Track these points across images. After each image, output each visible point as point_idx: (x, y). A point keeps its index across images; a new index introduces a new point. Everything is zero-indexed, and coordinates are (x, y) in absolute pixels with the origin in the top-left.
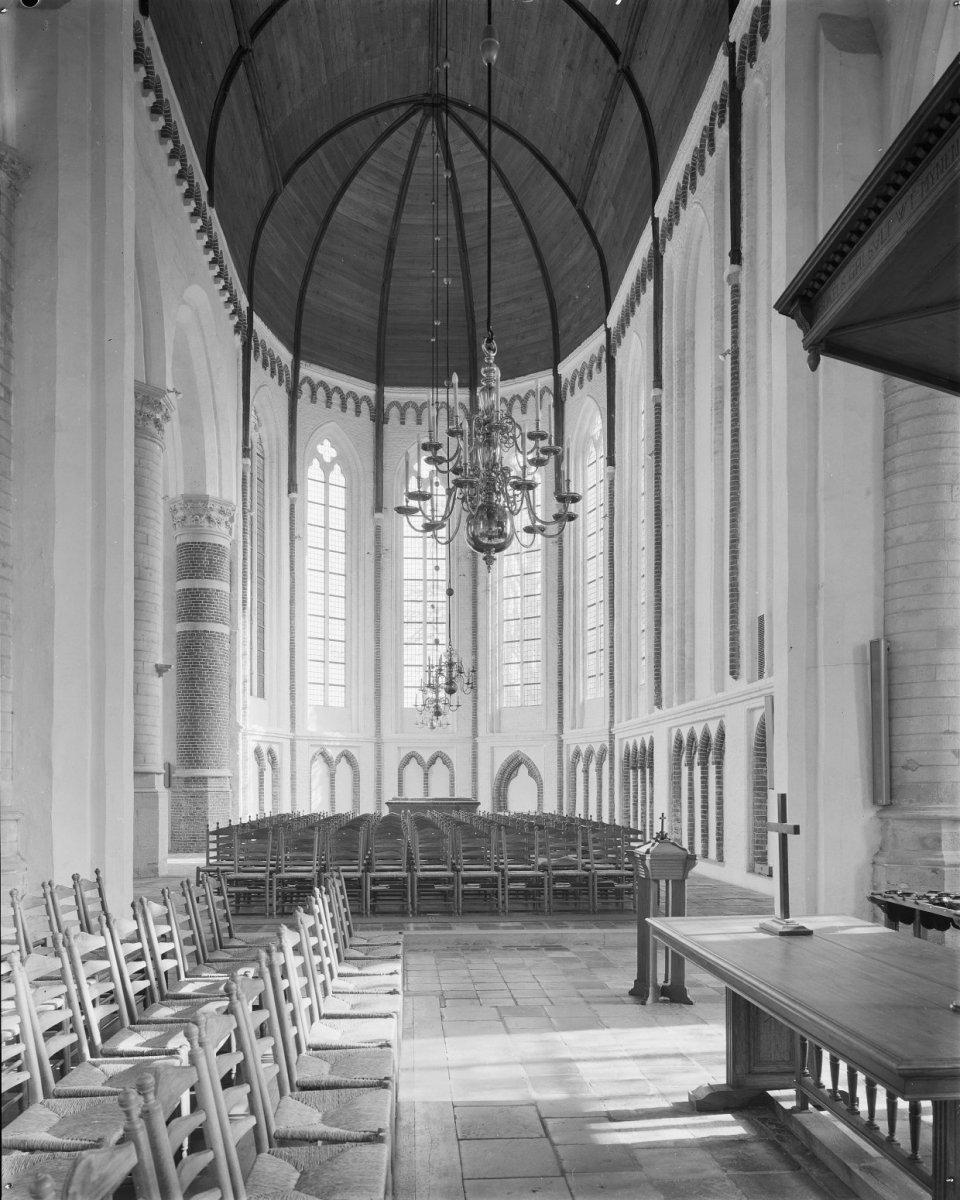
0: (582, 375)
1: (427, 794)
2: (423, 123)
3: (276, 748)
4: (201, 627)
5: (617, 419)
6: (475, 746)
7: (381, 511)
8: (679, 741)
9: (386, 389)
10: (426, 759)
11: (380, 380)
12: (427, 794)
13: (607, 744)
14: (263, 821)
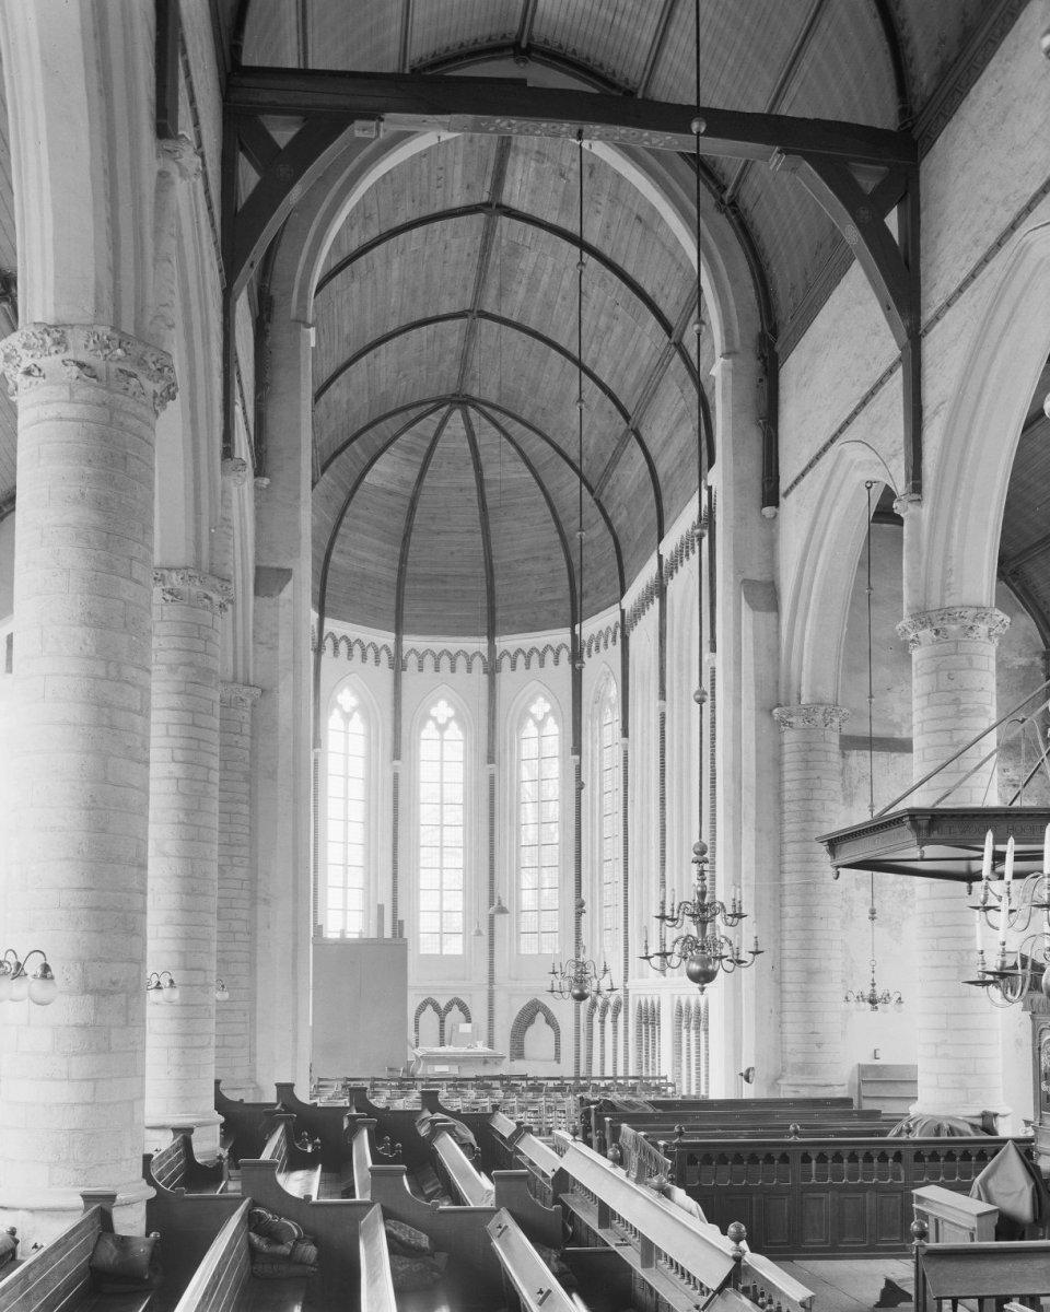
0: (599, 641)
2: (449, 413)
9: (405, 637)
10: (443, 1005)
13: (622, 998)
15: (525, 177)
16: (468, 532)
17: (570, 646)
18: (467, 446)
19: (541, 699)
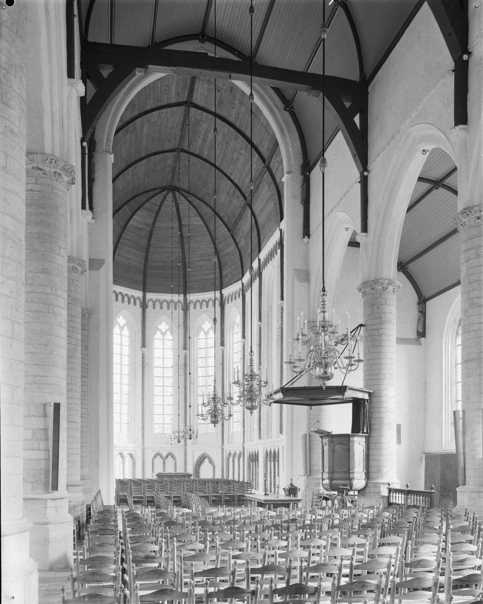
0: (232, 297)
1: (176, 471)
2: (167, 194)
5: (246, 320)
6: (186, 450)
7: (145, 347)
8: (267, 452)
10: (164, 455)
11: (145, 291)
13: (242, 451)
19: (207, 322)
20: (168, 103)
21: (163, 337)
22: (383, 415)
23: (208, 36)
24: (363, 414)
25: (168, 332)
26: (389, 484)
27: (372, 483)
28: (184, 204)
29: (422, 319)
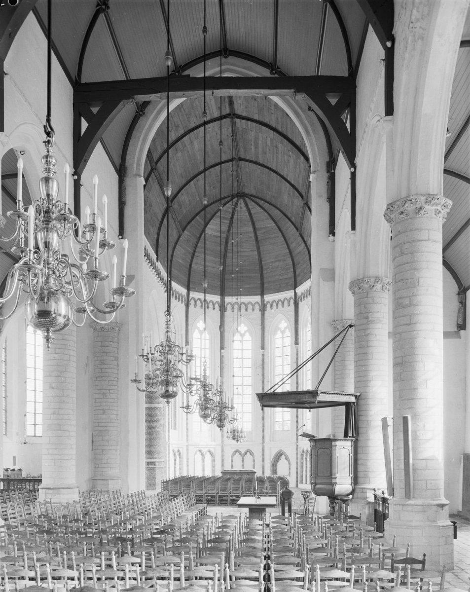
2: (237, 201)
3: (181, 450)
4: (153, 405)
9: (226, 298)
12: (243, 468)
14: (177, 479)
15: (241, 101)
16: (251, 251)
17: (293, 297)
18: (247, 214)
19: (283, 321)
20: (212, 118)
21: (242, 339)
22: (370, 418)
23: (230, 51)
24: (353, 415)
25: (247, 333)
26: (375, 490)
27: (358, 488)
28: (256, 210)
29: (462, 311)
